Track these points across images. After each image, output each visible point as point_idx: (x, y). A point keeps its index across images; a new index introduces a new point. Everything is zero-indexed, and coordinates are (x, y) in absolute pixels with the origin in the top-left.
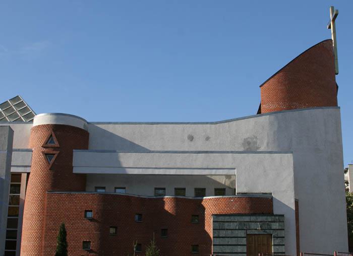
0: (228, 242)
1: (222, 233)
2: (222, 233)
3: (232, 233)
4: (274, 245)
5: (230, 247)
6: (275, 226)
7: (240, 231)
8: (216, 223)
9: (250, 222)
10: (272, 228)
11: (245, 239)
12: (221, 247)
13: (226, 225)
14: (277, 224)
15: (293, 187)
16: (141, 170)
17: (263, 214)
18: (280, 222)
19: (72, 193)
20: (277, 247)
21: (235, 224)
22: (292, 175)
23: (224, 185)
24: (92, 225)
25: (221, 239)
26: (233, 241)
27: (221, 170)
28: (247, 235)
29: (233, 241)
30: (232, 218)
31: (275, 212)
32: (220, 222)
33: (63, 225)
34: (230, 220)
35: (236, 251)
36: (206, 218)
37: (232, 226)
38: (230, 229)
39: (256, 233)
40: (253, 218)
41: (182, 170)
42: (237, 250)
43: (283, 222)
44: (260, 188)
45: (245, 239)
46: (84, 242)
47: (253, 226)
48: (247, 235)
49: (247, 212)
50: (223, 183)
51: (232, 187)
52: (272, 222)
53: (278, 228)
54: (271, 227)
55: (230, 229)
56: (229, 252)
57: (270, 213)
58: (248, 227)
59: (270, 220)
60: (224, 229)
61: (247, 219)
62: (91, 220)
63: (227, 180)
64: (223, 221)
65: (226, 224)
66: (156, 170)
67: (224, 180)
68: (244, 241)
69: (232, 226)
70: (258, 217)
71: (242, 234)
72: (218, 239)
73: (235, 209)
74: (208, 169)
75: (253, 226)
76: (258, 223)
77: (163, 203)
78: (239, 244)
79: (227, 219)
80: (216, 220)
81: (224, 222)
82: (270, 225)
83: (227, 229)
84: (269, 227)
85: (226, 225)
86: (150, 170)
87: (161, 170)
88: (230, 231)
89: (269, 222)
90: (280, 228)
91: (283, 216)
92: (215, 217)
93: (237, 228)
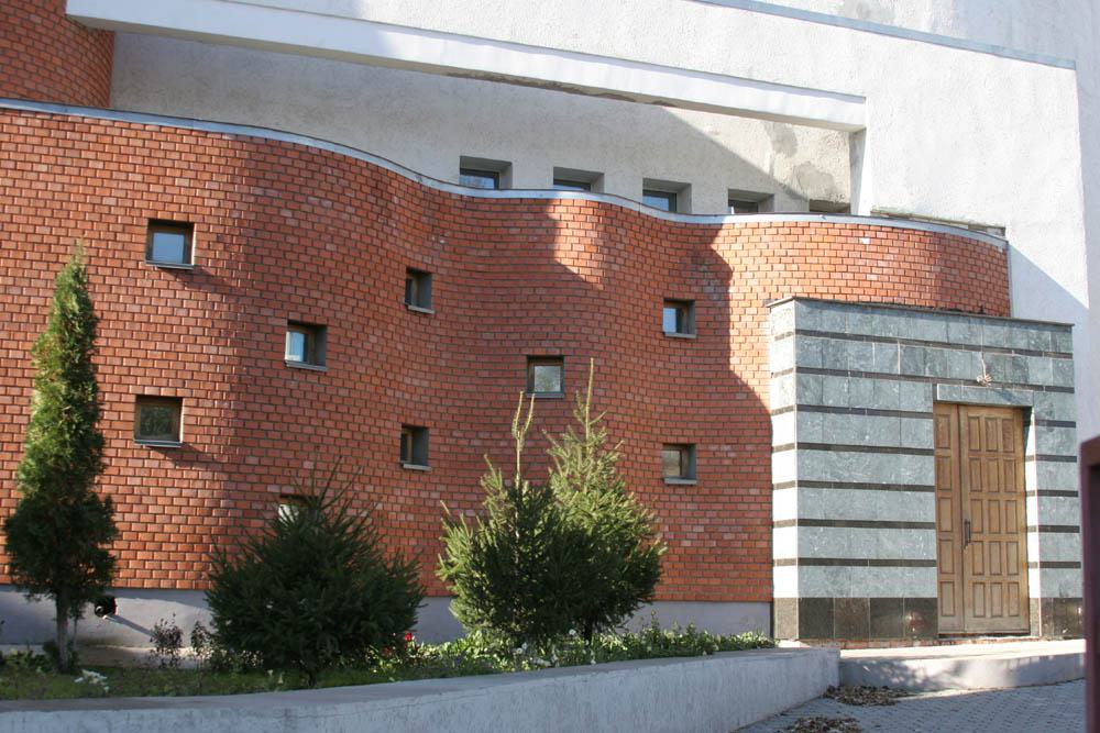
0: (863, 435)
1: (837, 391)
2: (837, 391)
3: (876, 390)
4: (1041, 458)
5: (868, 457)
6: (1042, 371)
7: (907, 385)
8: (809, 340)
9: (948, 345)
10: (1032, 381)
11: (928, 424)
12: (832, 455)
13: (852, 355)
14: (1050, 363)
15: (1078, 212)
16: (439, 43)
17: (981, 314)
18: (1059, 355)
19: (76, 114)
20: (1051, 466)
21: (889, 349)
22: (1076, 163)
23: (769, 178)
24: (189, 305)
25: (832, 416)
26: (878, 431)
27: (807, 99)
28: (937, 403)
29: (878, 431)
30: (875, 324)
31: (1020, 310)
32: (825, 334)
33: (80, 285)
34: (866, 331)
35: (892, 480)
36: (734, 318)
37: (877, 357)
38: (869, 375)
39: (973, 398)
40: (957, 330)
41: (635, 72)
42: (898, 476)
43: (1069, 356)
44: (961, 205)
45: (928, 424)
46: (141, 398)
47: (959, 364)
48: (937, 403)
49: (927, 299)
50: (766, 169)
51: (799, 191)
52: (1028, 352)
53: (1051, 382)
54: (1026, 378)
55: (869, 375)
56: (866, 480)
57: (997, 311)
58: (938, 369)
59: (1022, 344)
60: (843, 373)
61: (933, 329)
62: (188, 276)
63: (781, 156)
64: (837, 330)
65: (852, 348)
66: (514, 54)
67: (768, 155)
68: (924, 433)
69: (877, 357)
70: (976, 326)
71: (915, 397)
72: (819, 416)
73: (878, 276)
74: (750, 82)
75: (959, 364)
76: (979, 355)
77: (553, 228)
78: (905, 445)
79: (853, 322)
80: (808, 325)
81: (843, 336)
82: (1020, 367)
83: (856, 374)
84: (1018, 373)
85: (852, 355)
86: (487, 48)
87: (540, 58)
88: (867, 383)
89: (1019, 351)
90: (1060, 383)
91: (1066, 328)
92: (804, 308)
93: (898, 370)
